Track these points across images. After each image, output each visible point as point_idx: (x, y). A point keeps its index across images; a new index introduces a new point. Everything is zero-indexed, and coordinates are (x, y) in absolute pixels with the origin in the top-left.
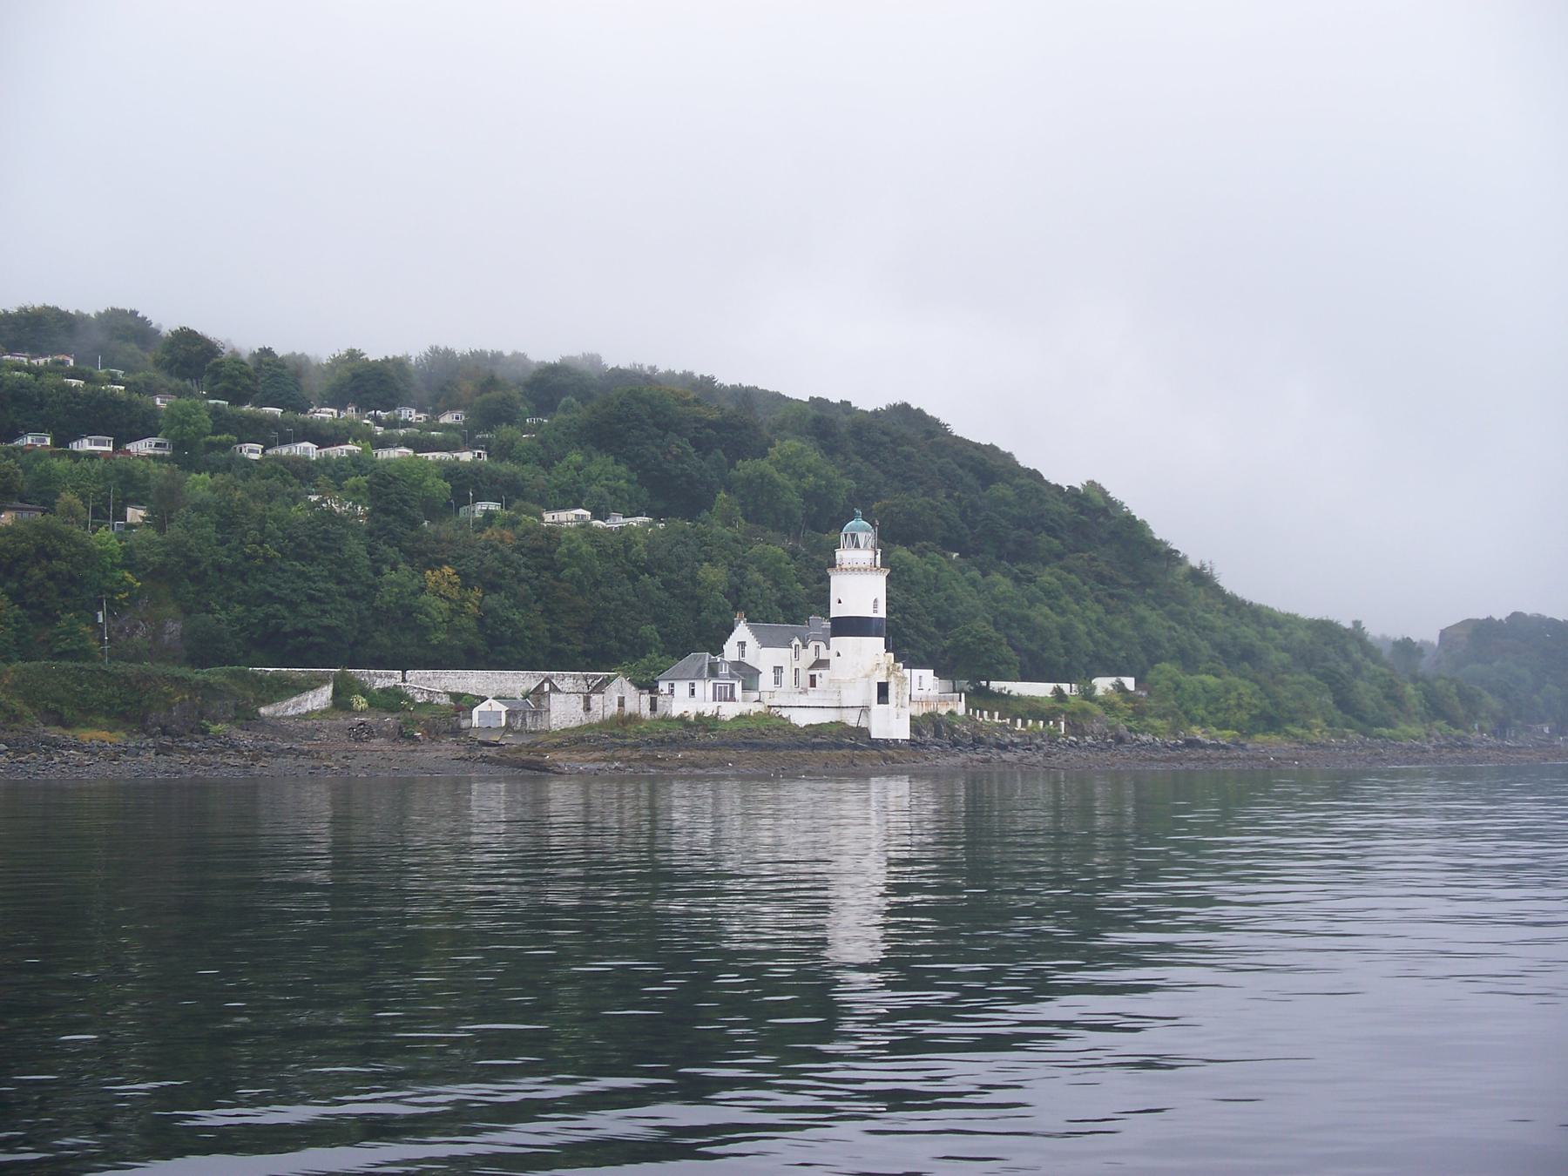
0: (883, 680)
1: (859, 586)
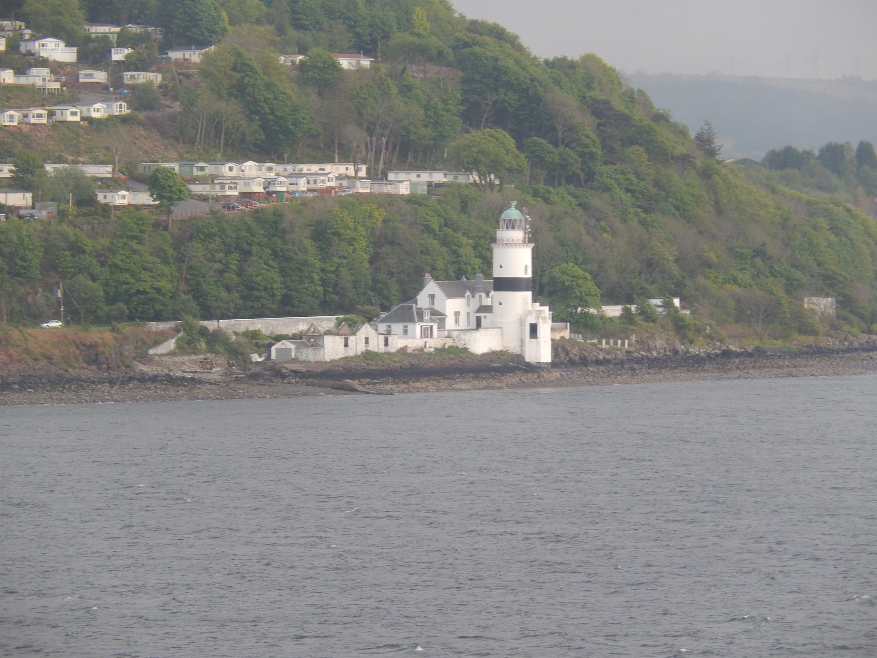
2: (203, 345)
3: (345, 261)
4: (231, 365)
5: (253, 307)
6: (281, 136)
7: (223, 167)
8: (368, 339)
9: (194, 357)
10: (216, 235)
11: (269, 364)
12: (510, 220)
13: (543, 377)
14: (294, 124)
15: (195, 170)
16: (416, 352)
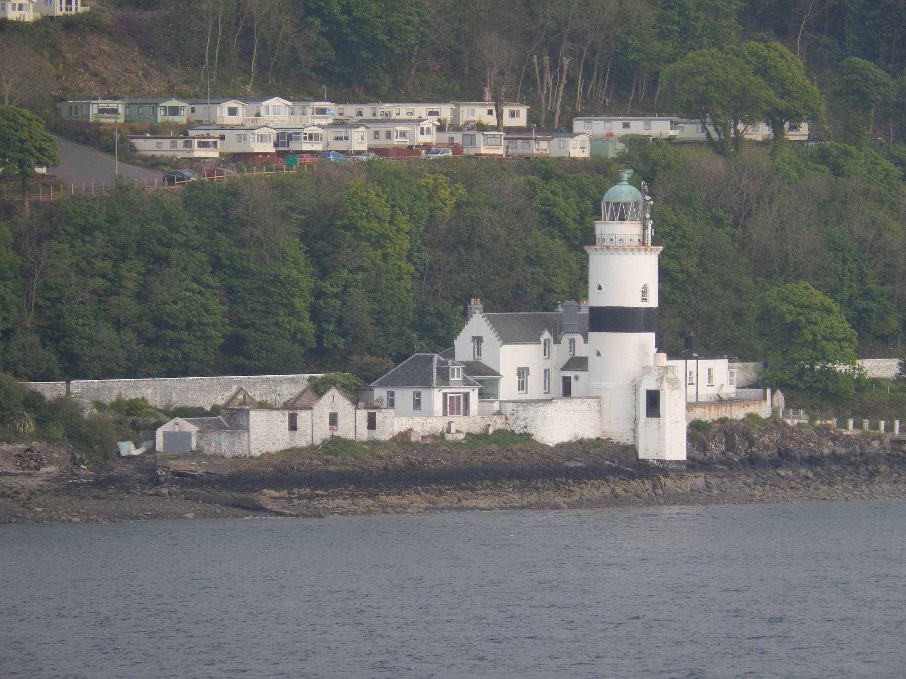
0: (653, 387)
1: (628, 271)
2: (30, 426)
3: (360, 276)
4: (76, 462)
5: (165, 359)
6: (364, 54)
7: (218, 108)
8: (335, 417)
10: (100, 228)
11: (149, 459)
12: (617, 204)
13: (663, 486)
14: (389, 32)
15: (161, 113)
16: (428, 441)
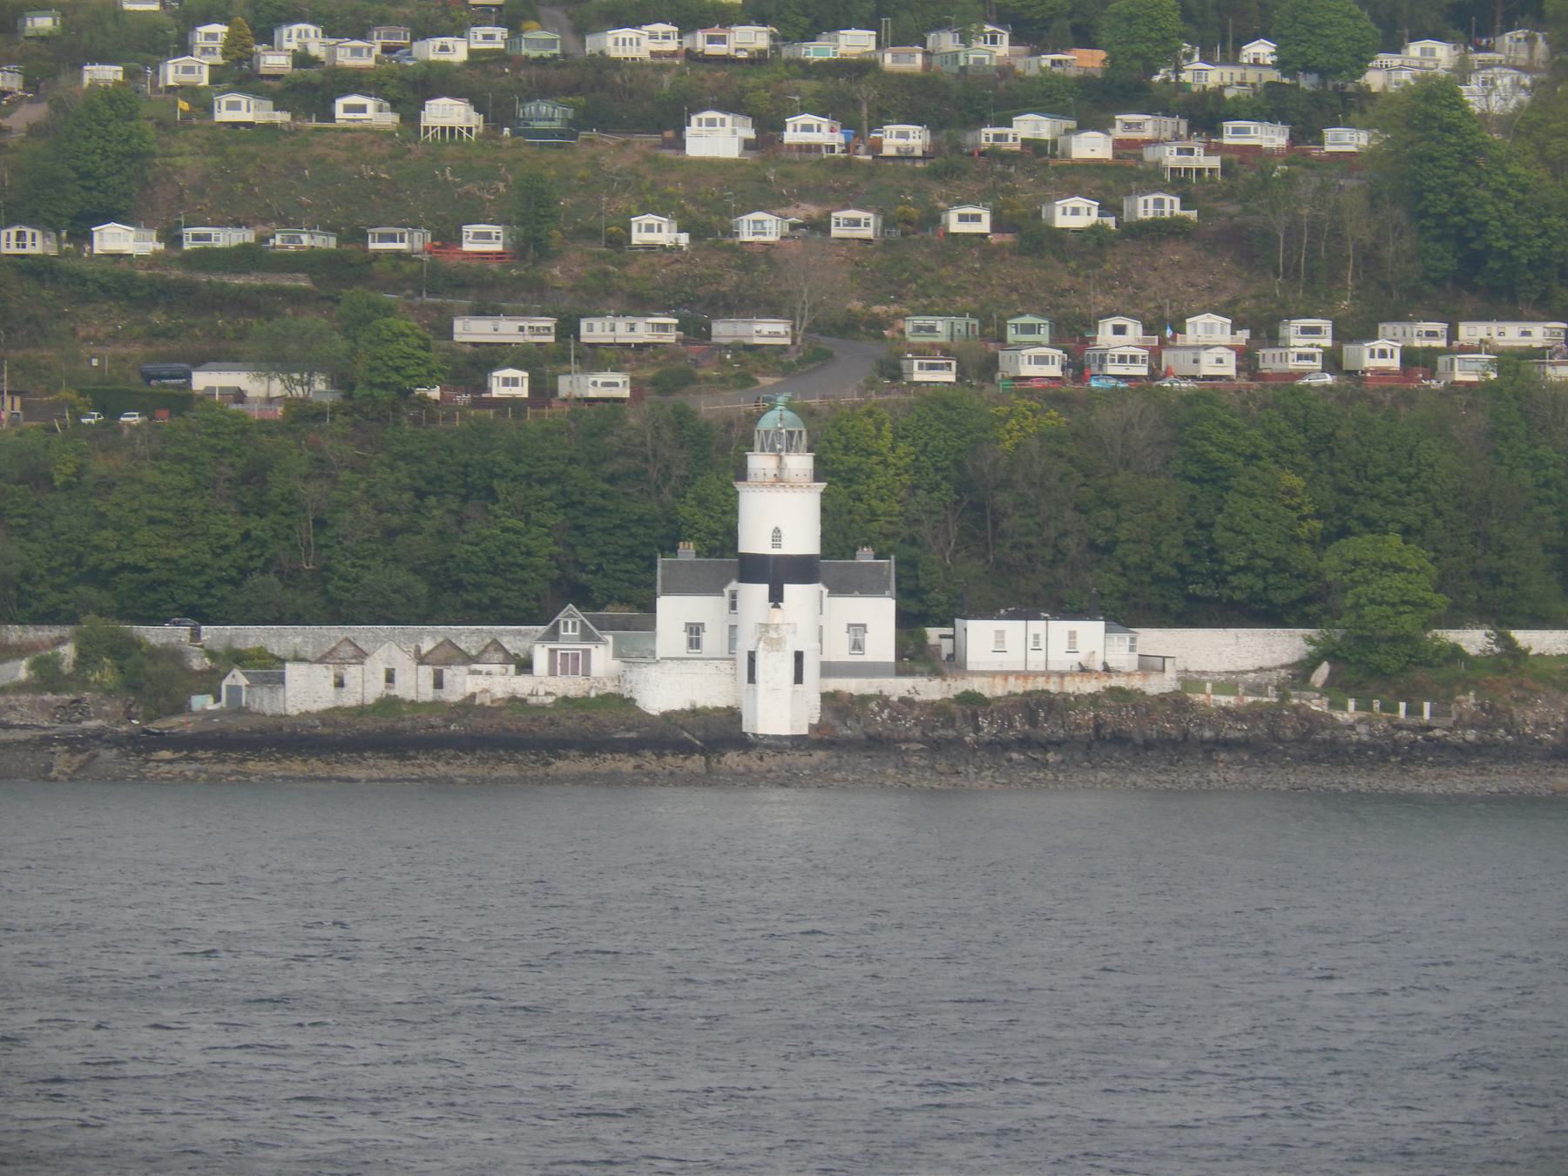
1: (780, 510)
9: (48, 697)
